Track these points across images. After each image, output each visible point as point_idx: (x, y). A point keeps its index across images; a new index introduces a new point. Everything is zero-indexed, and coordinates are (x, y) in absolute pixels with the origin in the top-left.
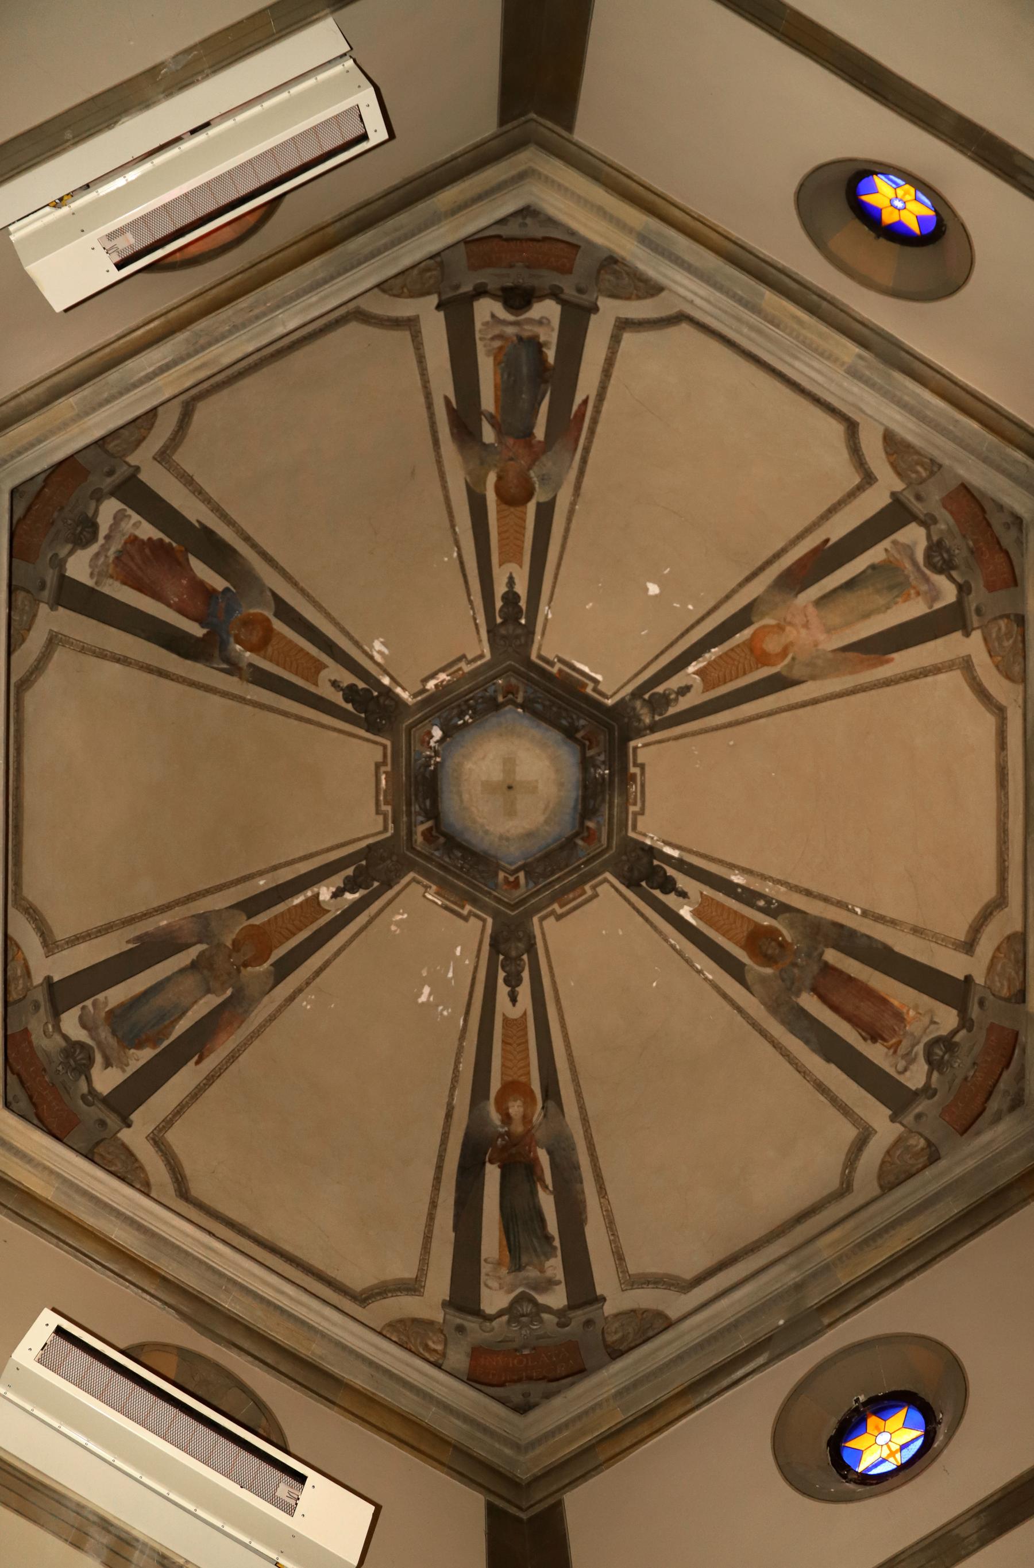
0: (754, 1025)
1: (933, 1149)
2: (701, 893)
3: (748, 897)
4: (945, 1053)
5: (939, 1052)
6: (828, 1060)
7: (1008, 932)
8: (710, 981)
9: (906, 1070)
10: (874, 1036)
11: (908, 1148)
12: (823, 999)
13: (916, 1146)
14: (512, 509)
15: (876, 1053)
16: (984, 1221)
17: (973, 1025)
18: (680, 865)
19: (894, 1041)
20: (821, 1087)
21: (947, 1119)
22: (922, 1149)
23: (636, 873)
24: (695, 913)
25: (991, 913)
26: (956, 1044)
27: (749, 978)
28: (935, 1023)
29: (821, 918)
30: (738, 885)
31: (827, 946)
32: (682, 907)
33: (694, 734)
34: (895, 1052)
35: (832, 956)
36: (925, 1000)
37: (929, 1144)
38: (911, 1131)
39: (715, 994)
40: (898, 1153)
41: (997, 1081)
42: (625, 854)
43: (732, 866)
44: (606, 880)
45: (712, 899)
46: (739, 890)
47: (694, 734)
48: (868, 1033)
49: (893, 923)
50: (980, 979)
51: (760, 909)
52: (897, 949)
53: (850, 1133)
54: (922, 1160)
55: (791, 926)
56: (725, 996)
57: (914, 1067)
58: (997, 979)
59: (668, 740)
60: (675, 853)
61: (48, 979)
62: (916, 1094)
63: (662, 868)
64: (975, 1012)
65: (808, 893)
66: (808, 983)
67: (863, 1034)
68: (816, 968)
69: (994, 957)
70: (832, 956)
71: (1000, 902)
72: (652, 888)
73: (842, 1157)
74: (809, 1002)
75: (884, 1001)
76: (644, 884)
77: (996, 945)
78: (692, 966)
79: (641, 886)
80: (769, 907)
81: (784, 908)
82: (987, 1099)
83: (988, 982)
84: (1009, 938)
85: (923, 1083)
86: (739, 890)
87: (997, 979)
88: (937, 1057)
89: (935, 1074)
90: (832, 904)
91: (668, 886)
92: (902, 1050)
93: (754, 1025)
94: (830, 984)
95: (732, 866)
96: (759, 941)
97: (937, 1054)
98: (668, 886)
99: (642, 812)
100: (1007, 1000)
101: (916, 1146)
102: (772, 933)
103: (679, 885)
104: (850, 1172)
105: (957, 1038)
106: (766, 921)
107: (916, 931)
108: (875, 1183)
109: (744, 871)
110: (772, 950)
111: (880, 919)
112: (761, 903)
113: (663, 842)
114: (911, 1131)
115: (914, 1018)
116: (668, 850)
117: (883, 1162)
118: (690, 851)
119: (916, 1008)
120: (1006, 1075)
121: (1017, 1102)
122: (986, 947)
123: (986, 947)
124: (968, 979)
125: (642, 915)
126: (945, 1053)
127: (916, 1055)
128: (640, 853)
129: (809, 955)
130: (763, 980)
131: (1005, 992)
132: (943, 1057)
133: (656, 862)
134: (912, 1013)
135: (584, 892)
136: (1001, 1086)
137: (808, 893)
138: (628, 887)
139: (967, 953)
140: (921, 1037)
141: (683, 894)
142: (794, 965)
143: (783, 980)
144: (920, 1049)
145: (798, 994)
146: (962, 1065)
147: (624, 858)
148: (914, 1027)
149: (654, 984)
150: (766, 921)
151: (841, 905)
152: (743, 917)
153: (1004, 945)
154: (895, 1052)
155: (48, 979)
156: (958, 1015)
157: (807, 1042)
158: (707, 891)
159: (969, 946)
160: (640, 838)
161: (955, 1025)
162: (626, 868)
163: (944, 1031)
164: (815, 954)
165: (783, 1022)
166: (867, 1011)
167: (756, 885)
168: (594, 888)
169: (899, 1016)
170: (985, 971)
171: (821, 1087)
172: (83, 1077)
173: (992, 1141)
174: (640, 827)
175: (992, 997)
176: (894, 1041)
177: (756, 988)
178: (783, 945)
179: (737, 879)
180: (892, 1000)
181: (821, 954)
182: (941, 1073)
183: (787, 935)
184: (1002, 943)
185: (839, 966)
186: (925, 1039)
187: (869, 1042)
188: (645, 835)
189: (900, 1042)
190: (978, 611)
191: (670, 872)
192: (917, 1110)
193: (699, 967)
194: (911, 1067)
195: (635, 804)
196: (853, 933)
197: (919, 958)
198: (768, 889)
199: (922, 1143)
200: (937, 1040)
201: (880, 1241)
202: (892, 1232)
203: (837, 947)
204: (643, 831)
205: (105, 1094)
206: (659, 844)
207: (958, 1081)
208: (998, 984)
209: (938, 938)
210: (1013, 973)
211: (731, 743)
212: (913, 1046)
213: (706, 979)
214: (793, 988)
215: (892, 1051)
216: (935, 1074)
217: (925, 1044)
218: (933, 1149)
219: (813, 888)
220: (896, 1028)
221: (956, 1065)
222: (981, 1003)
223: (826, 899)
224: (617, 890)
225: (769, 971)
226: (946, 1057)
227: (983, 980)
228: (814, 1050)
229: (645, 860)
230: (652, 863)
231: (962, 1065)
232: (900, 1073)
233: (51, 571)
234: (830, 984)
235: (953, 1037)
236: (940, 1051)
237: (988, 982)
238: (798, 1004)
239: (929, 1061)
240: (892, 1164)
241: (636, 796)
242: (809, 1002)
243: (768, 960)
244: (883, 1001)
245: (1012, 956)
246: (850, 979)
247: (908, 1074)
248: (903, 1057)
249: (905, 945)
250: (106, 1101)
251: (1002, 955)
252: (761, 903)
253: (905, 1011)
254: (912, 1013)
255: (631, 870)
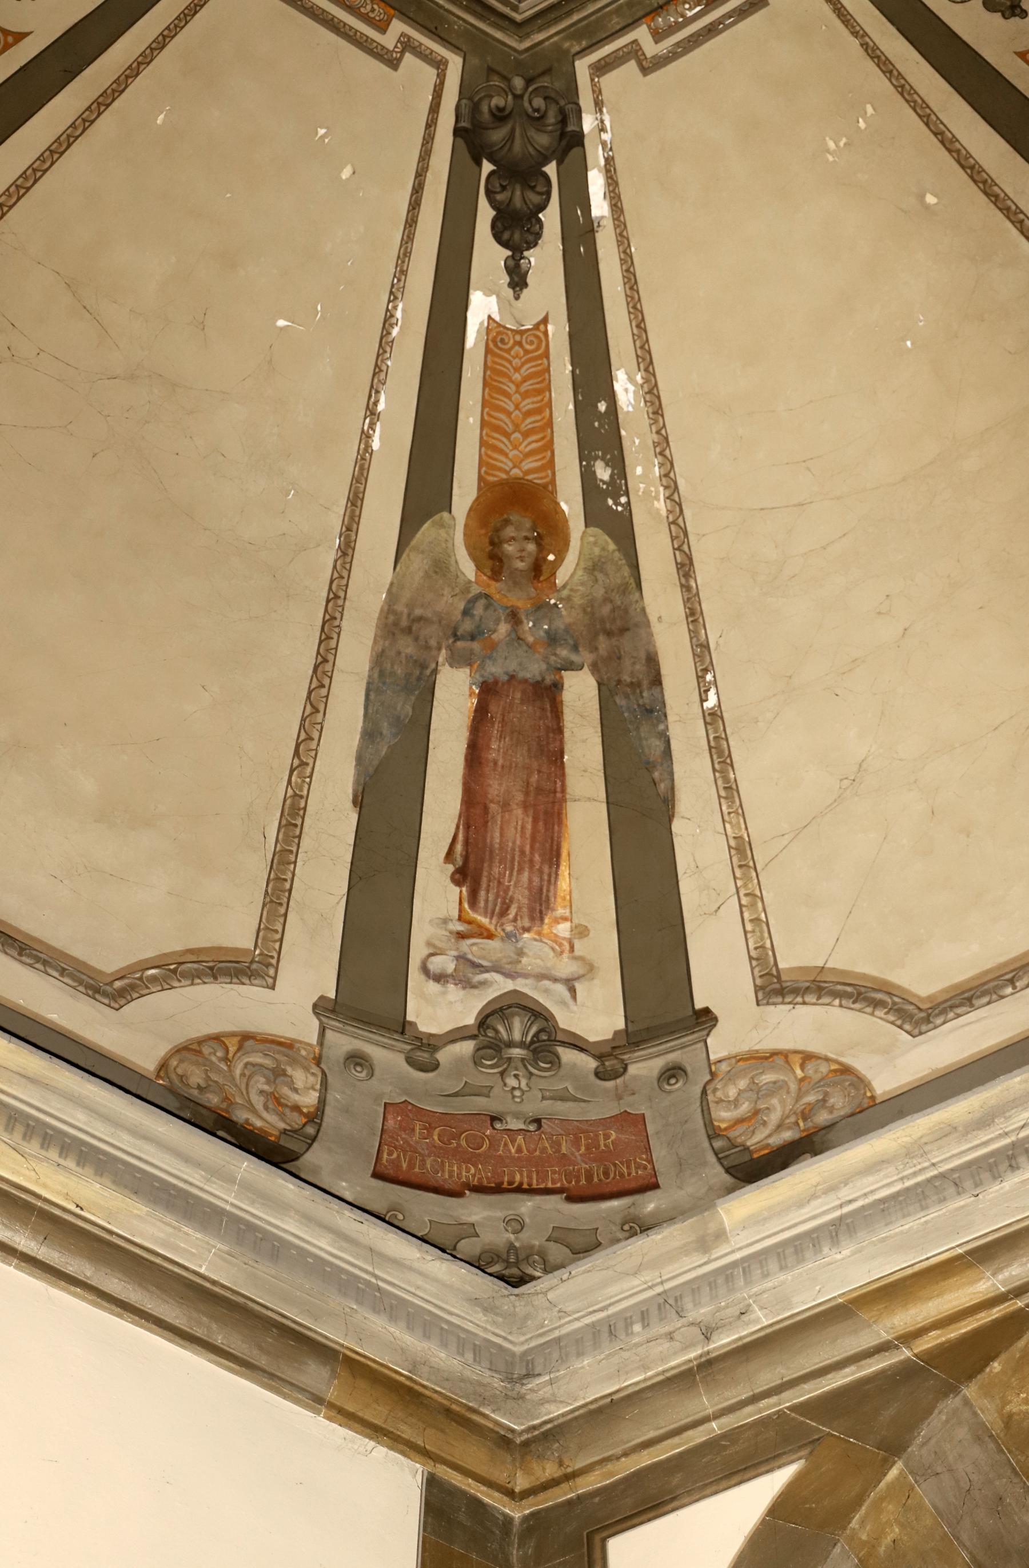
0: (336, 598)
1: (310, 1130)
2: (545, 321)
3: (600, 435)
4: (522, 1045)
5: (518, 1029)
6: (359, 801)
7: (860, 1063)
8: (368, 446)
9: (440, 978)
10: (467, 873)
11: (278, 1074)
12: (480, 718)
13: (296, 1090)
14: (516, 472)
15: (435, 896)
16: (219, 1340)
17: (615, 1075)
18: (579, 235)
19: (485, 921)
20: (293, 815)
21: (391, 1123)
22: (296, 1108)
23: (497, 136)
24: (494, 332)
25: (877, 1004)
26: (555, 1062)
27: (427, 531)
28: (573, 991)
29: (648, 624)
30: (611, 398)
31: (595, 669)
32: (488, 292)
33: (904, 90)
34: (461, 936)
35: (580, 691)
36: (604, 945)
37: (316, 1117)
38: (318, 1061)
39: (348, 470)
40: (257, 1059)
41: (531, 1191)
42: (529, 81)
43: (645, 360)
44: (440, 65)
45: (546, 355)
46: (602, 407)
47: (904, 90)
48: (466, 858)
49: (730, 791)
50: (720, 1044)
51: (588, 477)
52: (677, 826)
53: (238, 932)
54: (272, 1118)
55: (595, 567)
56: (356, 500)
57: (454, 993)
58: (743, 1084)
59: (857, 32)
60: (599, 207)
61: (321, 1007)
62: (403, 1027)
63: (548, 194)
64: (644, 1067)
65: (685, 568)
66: (496, 669)
67: (459, 848)
68: (534, 669)
69: (785, 1055)
70: (580, 691)
71: (917, 1016)
72: (489, 193)
73: (175, 945)
74: (454, 695)
75: (553, 856)
76: (487, 167)
77: (811, 1048)
78: (374, 390)
79: (479, 164)
80: (606, 494)
81: (621, 530)
82: (479, 1189)
83: (724, 1067)
84: (846, 1070)
85: (433, 1030)
86: (602, 407)
87: (743, 1084)
88: (504, 1034)
89: (467, 1048)
90: (693, 634)
91: (517, 230)
92: (473, 948)
93: (336, 598)
94: (519, 716)
95: (645, 360)
96: (516, 505)
97: (509, 1029)
98: (517, 230)
99: (648, 67)
100: (713, 1133)
101: (296, 1090)
102: (549, 530)
103: (533, 257)
104: (154, 979)
105: (567, 1055)
106: (570, 503)
107: (742, 851)
108: (162, 1050)
109: (652, 394)
110: (518, 551)
111: (720, 755)
112: (603, 473)
113: (609, 161)
114: (318, 1061)
115: (556, 939)
116: (596, 183)
117: (217, 1038)
118: (623, 240)
119: (581, 932)
120: (555, 1202)
121: (511, 1269)
122: (798, 1026)
123: (798, 1026)
124: (706, 1018)
125: (415, 205)
126: (522, 1045)
127: (483, 984)
128: (551, 119)
129: (552, 639)
130: (441, 567)
131: (723, 1116)
132: (510, 1044)
133: (551, 169)
134: (563, 929)
135: (382, 27)
136: (526, 1206)
137: (685, 568)
138: (457, 132)
139: (757, 989)
140: (526, 976)
141: (518, 279)
142: (514, 617)
143: (466, 612)
144: (500, 985)
145: (457, 660)
146: (519, 1095)
147: (518, 83)
148: (536, 951)
149: (281, 323)
150: (570, 503)
151: (701, 651)
152: (549, 446)
153: (824, 1068)
154: (461, 936)
155: (321, 1007)
156: (617, 1033)
157: (370, 734)
158: (558, 332)
159: (775, 987)
160: (586, 99)
161: (592, 1039)
162: (497, 101)
163: (566, 1019)
164: (564, 652)
165: (379, 660)
166: (512, 829)
167: (636, 439)
168: (407, 45)
169: (540, 905)
170: (744, 1047)
171: (293, 815)
172: (560, 1050)
173: (397, 1263)
174: (609, 81)
175: (698, 1090)
176: (485, 921)
177: (417, 563)
178: (539, 571)
179: (626, 389)
180: (564, 870)
181: (571, 666)
182: (477, 1060)
183: (567, 570)
184: (827, 1059)
185: (569, 718)
186: (524, 986)
187: (451, 868)
188: (599, 105)
189: (490, 936)
190: (357, 1060)
191: (551, 218)
192: (369, 1049)
193: (381, 407)
194: (451, 987)
195: (658, 36)
196: (654, 712)
197: (687, 887)
198: (643, 472)
199: (309, 1100)
200: (537, 1013)
201: (33, 1147)
202: (70, 1163)
203: (607, 693)
204: (606, 96)
205: (621, 1024)
206: (596, 156)
207: (480, 1104)
208: (732, 1092)
209: (752, 904)
210: (774, 1118)
211: (931, 199)
212: (496, 969)
213: (366, 437)
214: (465, 640)
215: (460, 927)
216: (467, 1048)
217: (515, 992)
218: (310, 1130)
219: (704, 575)
220: (513, 912)
221: (512, 1082)
222: (673, 1072)
223: (694, 615)
224: (435, 108)
225: (468, 569)
226: (517, 1052)
227: (723, 1054)
228: (359, 759)
229: (543, 140)
230: (546, 161)
231: (519, 1095)
232: (425, 970)
233: (632, 1069)
234: (519, 716)
235: (563, 1044)
236: (520, 1034)
237: (724, 1067)
238: (435, 672)
239: (484, 1022)
240: (226, 1059)
241: (678, 27)
242: (454, 695)
243: (492, 559)
244: (550, 851)
245: (811, 1098)
246: (557, 758)
247: (433, 987)
248: (461, 958)
249: (697, 842)
250: (636, 1036)
251: (799, 1073)
252: (603, 473)
253: (560, 911)
254: (563, 929)
255: (500, 116)
